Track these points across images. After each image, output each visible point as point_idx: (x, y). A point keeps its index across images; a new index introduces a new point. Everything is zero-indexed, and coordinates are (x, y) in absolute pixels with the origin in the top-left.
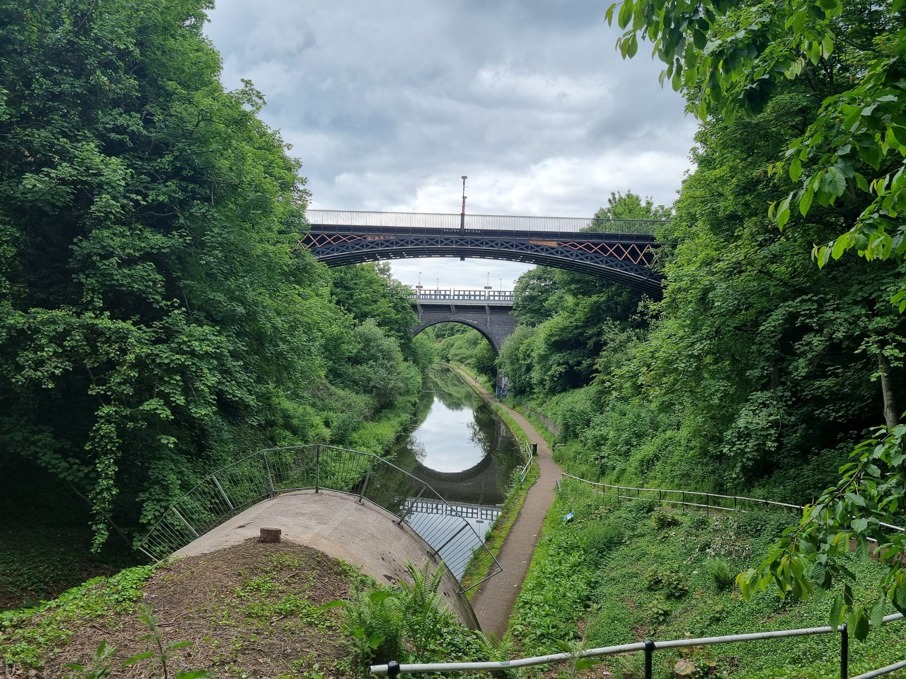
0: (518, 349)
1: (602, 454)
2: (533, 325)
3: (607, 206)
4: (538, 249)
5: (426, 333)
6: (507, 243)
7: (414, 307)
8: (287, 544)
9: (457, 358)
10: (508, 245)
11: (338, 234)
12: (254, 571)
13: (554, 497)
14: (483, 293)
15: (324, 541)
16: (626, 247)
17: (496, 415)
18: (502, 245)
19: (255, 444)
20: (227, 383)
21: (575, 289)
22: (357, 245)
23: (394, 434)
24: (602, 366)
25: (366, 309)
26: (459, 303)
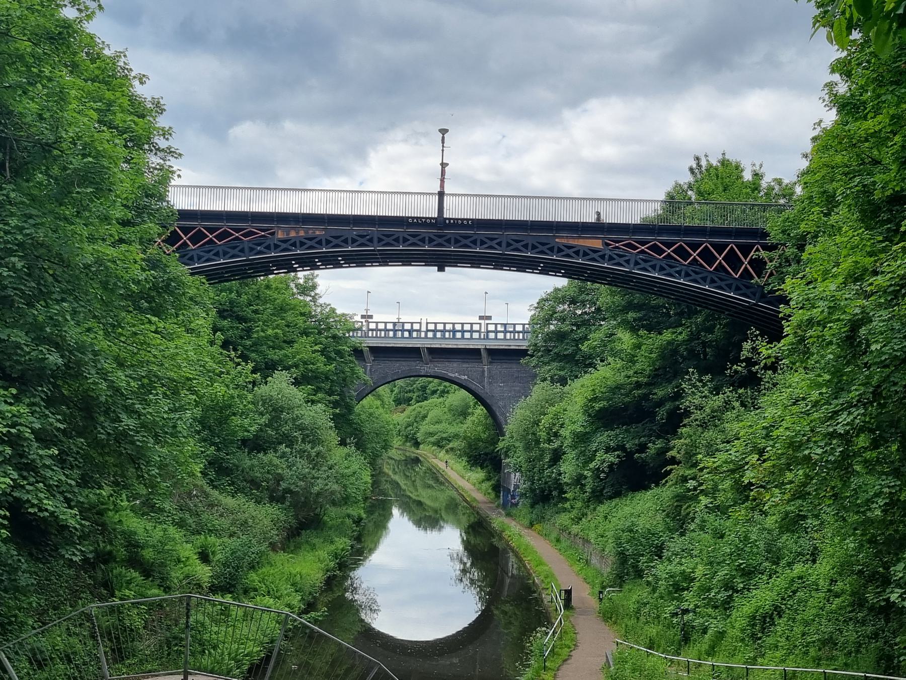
0: (537, 423)
1: (685, 606)
2: (563, 381)
4: (570, 252)
5: (379, 397)
6: (517, 241)
9: (432, 439)
10: (519, 245)
11: (225, 226)
14: (476, 327)
16: (720, 248)
17: (501, 538)
18: (509, 245)
21: (635, 320)
24: (683, 452)
26: (436, 344)
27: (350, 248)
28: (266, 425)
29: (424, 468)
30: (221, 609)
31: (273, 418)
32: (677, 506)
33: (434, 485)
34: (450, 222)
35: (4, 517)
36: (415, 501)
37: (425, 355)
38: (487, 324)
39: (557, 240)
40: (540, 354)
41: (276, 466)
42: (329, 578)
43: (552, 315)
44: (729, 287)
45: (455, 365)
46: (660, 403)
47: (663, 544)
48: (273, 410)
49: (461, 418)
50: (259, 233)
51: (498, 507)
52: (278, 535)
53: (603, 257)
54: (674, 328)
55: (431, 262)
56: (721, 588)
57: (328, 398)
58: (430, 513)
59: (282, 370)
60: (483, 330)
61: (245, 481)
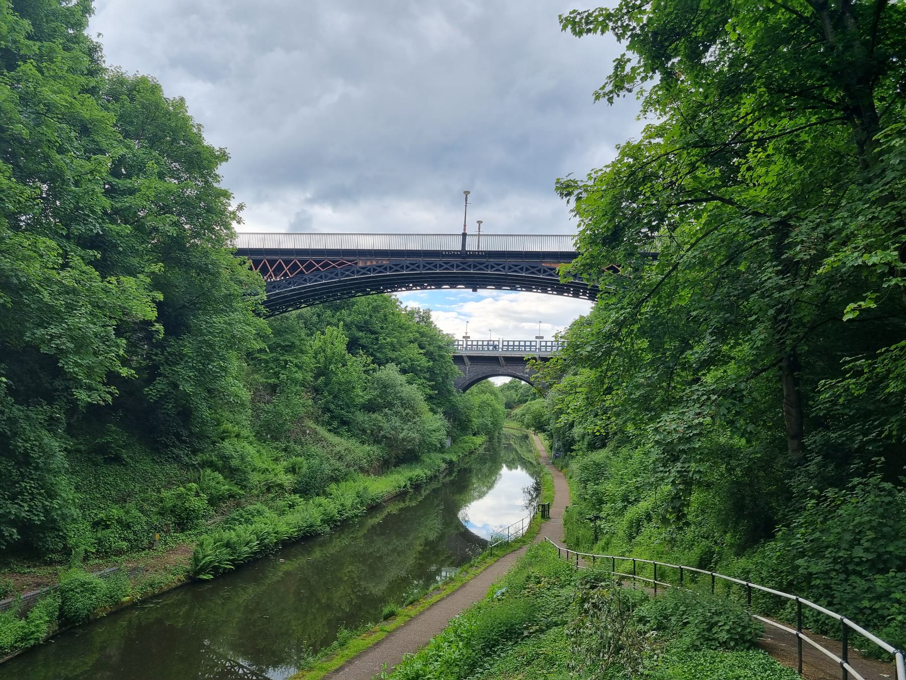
6: (516, 266)
10: (517, 269)
11: (326, 259)
14: (534, 344)
26: (508, 354)
37: (502, 361)
57: (428, 383)
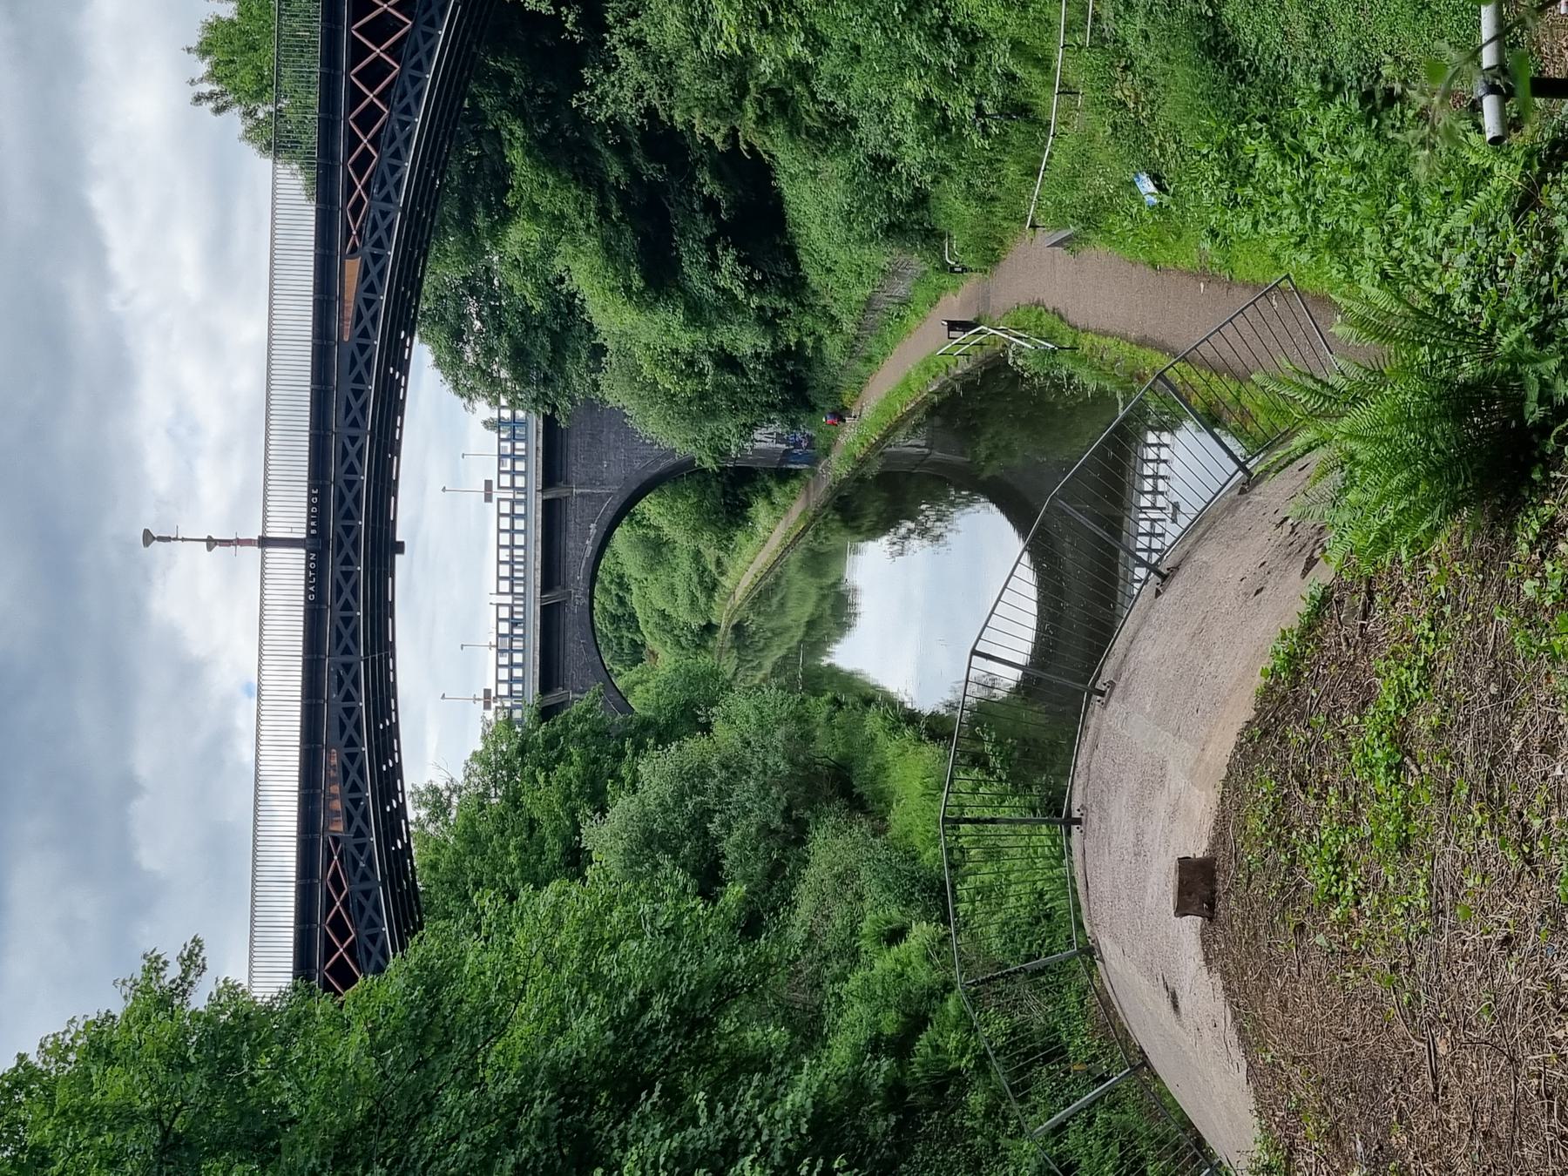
0: (671, 397)
1: (970, 113)
2: (599, 351)
3: (234, 118)
4: (367, 315)
5: (630, 689)
6: (349, 408)
7: (546, 713)
8: (1219, 838)
9: (702, 600)
11: (322, 926)
12: (1290, 895)
13: (1098, 251)
14: (505, 507)
15: (1209, 753)
16: (359, 52)
17: (863, 461)
18: (355, 424)
19: (956, 1135)
20: (764, 1138)
21: (489, 215)
22: (355, 863)
23: (924, 749)
24: (715, 122)
25: (554, 848)
26: (536, 577)
27: (362, 704)
28: (675, 858)
29: (751, 616)
30: (981, 900)
31: (662, 846)
32: (808, 134)
33: (780, 596)
34: (313, 528)
35: (812, 1167)
36: (807, 634)
37: (554, 596)
38: (499, 487)
39: (346, 338)
40: (551, 394)
41: (744, 836)
42: (931, 738)
43: (483, 372)
44: (428, 37)
45: (571, 544)
46: (634, 172)
47: (870, 157)
48: (648, 846)
49: (664, 550)
50: (336, 865)
51: (814, 473)
52: (860, 825)
53: (376, 258)
54: (501, 144)
55: (386, 566)
56: (941, 47)
57: (629, 757)
58: (827, 606)
59: (580, 835)
60: (511, 496)
61: (769, 888)
